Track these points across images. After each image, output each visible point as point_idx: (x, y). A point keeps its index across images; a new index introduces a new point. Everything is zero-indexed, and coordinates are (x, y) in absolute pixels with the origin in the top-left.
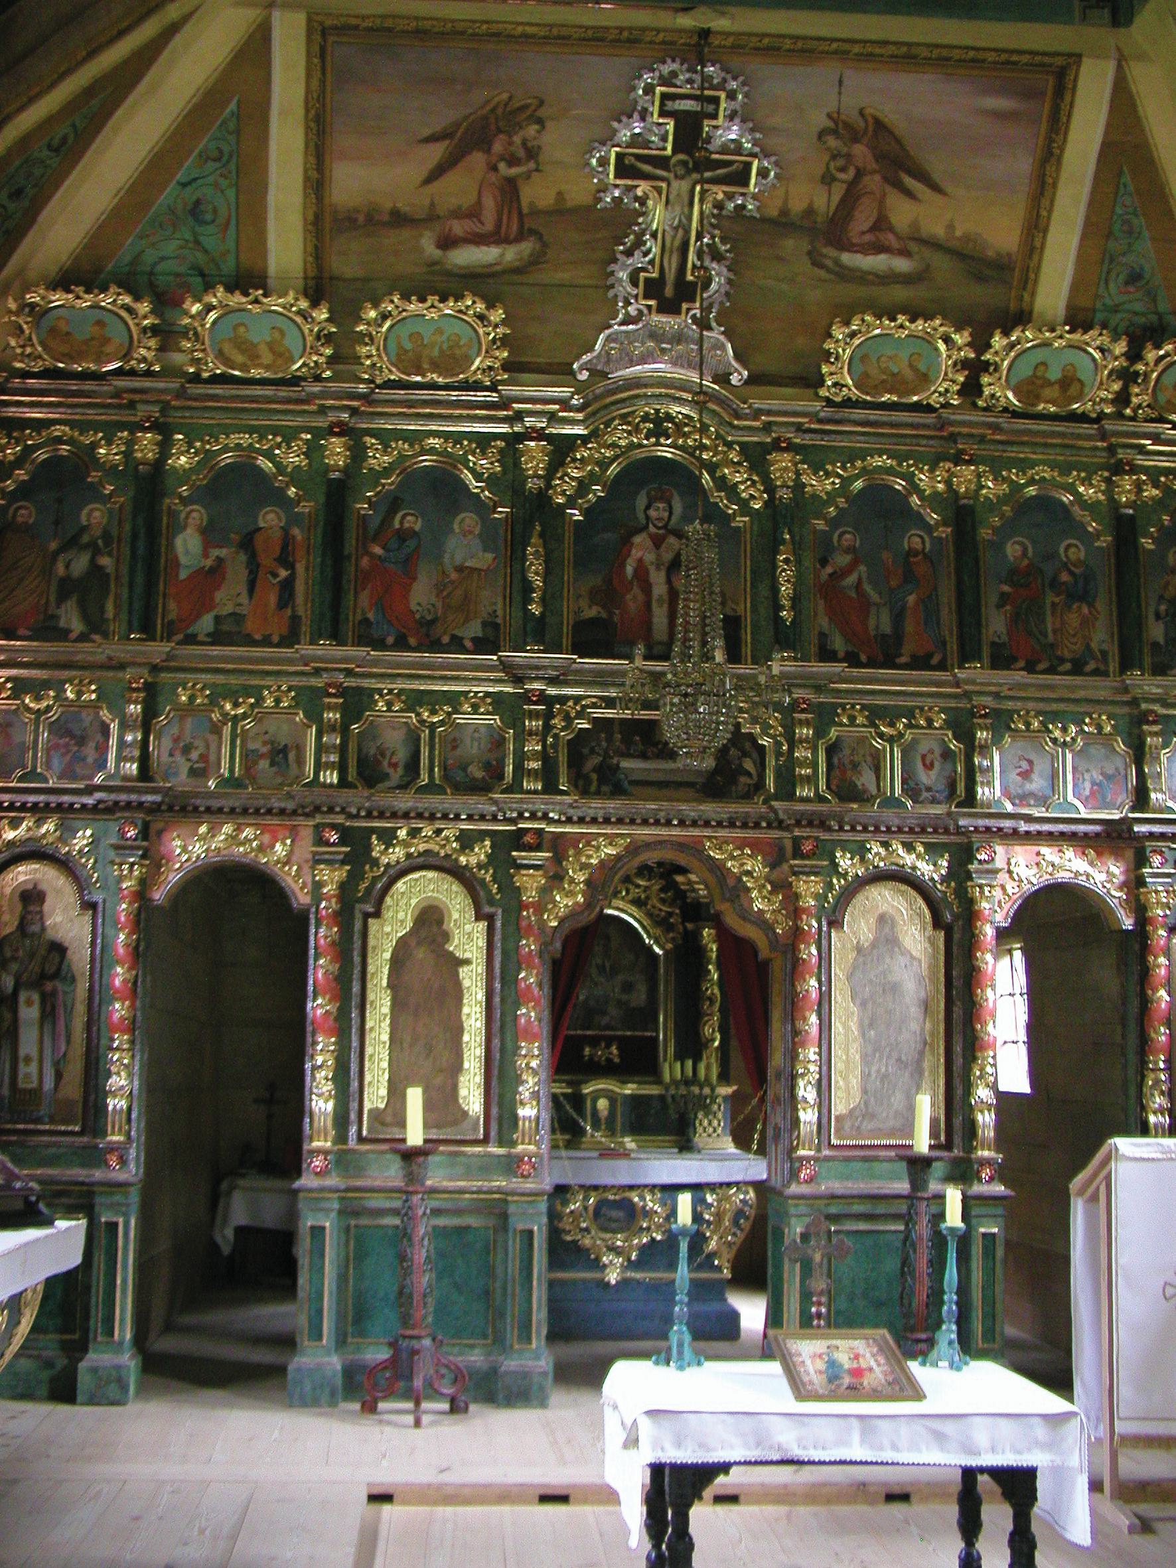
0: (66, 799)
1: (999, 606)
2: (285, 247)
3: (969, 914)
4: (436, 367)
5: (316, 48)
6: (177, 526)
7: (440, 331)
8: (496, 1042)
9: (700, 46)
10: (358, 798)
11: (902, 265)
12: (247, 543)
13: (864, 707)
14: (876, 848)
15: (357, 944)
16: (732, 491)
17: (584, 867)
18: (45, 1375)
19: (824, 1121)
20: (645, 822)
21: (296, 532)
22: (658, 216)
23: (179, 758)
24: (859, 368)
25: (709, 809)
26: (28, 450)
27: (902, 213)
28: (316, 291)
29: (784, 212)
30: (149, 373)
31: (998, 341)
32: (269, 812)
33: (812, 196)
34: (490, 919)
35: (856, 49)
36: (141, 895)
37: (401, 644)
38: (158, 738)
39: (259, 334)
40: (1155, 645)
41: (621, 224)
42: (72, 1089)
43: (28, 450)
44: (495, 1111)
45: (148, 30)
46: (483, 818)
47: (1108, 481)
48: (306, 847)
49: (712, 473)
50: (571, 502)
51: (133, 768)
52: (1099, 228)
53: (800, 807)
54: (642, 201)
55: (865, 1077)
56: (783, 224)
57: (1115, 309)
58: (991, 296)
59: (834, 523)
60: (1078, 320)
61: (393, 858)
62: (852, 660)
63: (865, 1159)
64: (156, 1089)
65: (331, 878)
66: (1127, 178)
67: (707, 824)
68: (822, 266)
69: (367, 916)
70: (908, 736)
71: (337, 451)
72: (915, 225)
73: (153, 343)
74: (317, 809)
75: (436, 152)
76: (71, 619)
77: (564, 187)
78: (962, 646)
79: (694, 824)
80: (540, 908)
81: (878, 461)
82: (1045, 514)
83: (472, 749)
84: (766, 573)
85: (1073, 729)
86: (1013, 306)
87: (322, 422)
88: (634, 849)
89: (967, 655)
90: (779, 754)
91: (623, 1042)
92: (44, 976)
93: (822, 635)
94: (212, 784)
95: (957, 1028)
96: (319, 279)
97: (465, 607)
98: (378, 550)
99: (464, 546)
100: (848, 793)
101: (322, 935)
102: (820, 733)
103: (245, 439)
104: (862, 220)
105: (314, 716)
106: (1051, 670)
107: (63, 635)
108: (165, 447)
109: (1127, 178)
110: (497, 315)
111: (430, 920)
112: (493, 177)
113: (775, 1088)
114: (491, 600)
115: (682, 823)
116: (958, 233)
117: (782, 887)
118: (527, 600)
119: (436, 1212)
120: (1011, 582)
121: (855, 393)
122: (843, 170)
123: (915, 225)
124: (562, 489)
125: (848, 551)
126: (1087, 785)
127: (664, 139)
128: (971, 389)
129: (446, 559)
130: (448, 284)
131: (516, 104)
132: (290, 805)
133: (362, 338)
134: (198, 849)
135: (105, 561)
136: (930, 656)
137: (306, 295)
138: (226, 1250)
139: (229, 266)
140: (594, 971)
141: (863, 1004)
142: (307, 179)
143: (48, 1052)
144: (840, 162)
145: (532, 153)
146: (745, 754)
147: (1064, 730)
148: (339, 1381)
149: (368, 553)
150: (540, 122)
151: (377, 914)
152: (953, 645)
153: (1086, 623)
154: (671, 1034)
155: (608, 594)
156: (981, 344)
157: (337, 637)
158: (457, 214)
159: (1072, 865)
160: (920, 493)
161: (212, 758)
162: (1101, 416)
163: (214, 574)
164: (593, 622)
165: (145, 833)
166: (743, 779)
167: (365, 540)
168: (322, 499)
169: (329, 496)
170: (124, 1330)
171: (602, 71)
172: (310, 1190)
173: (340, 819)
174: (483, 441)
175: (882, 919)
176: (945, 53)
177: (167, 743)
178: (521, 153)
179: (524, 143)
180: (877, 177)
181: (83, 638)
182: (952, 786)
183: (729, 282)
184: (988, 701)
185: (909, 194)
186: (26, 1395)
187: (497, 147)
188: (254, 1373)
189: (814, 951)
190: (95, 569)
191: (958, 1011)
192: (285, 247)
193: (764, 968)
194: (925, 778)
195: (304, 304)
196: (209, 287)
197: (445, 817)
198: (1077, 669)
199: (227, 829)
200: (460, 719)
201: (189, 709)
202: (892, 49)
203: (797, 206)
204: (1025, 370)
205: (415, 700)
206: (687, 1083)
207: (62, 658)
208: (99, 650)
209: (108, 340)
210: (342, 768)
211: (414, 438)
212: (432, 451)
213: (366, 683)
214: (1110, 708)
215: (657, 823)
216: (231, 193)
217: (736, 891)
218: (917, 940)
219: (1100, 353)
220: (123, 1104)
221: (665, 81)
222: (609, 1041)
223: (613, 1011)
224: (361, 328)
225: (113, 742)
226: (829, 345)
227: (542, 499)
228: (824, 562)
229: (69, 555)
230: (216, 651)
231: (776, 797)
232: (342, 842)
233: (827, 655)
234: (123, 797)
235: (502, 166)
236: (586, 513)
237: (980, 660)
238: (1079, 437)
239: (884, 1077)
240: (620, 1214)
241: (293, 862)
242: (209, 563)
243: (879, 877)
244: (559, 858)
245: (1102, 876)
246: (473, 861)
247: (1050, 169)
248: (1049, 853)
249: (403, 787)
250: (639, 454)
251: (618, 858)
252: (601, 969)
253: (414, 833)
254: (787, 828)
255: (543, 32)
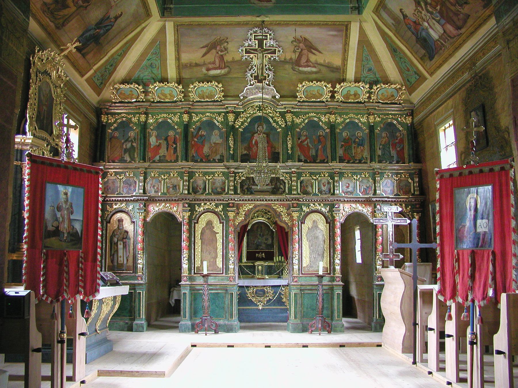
0: (127, 198)
1: (341, 148)
2: (172, 72)
3: (334, 220)
4: (207, 97)
5: (176, 29)
6: (150, 136)
7: (208, 89)
8: (225, 251)
9: (262, 25)
10: (191, 197)
11: (314, 70)
12: (166, 139)
13: (309, 172)
14: (312, 205)
15: (193, 230)
16: (277, 123)
17: (244, 211)
18: (126, 325)
19: (300, 268)
20: (258, 200)
21: (177, 136)
22: (255, 62)
23: (152, 188)
24: (305, 94)
25: (273, 197)
26: (116, 120)
27: (312, 58)
28: (179, 81)
29: (285, 59)
30: (143, 102)
31: (338, 86)
32: (172, 200)
33: (290, 55)
34: (223, 223)
35: (298, 23)
36: (144, 220)
37: (201, 161)
38: (147, 184)
39: (167, 92)
40: (379, 156)
41: (247, 65)
42: (130, 263)
43: (116, 120)
44: (224, 267)
45: (138, 29)
46: (220, 200)
47: (367, 117)
48: (181, 208)
49: (272, 119)
50: (240, 127)
51: (142, 191)
52: (359, 59)
53: (292, 196)
54: (252, 59)
55: (310, 258)
56: (285, 62)
57: (366, 77)
58: (336, 76)
59: (301, 129)
60: (357, 81)
61: (200, 210)
62: (306, 162)
63: (310, 277)
64: (149, 263)
65: (187, 215)
66: (365, 48)
67: (272, 200)
68: (295, 71)
69: (195, 223)
70: (319, 179)
71: (186, 118)
72: (316, 60)
73: (143, 95)
74: (183, 199)
75: (204, 50)
76: (127, 158)
77: (234, 56)
78: (332, 157)
79: (269, 200)
80: (234, 221)
81: (312, 114)
82: (353, 125)
83: (218, 184)
84: (285, 142)
85: (359, 176)
86: (341, 78)
87: (183, 111)
88: (255, 207)
89: (333, 159)
90: (289, 184)
91: (266, 253)
92: (123, 238)
93: (299, 156)
94: (160, 194)
95: (332, 246)
96: (180, 78)
97: (216, 152)
98: (196, 140)
99: (216, 138)
100: (305, 193)
101: (185, 228)
102: (298, 178)
103: (165, 115)
104: (303, 60)
105: (182, 178)
106: (353, 163)
107: (125, 161)
108: (147, 118)
109: (365, 48)
110: (220, 85)
111: (209, 223)
112: (217, 55)
113: (290, 261)
114: (222, 150)
115: (266, 200)
116: (327, 62)
117: (289, 214)
118: (230, 150)
119: (210, 289)
120: (344, 142)
121: (305, 99)
122: (298, 49)
123: (316, 60)
124: (238, 124)
125: (304, 136)
126: (363, 189)
127: (256, 45)
128: (333, 97)
129: (211, 141)
130: (208, 79)
131: (222, 39)
132: (177, 199)
133: (190, 92)
134: (157, 209)
135: (134, 144)
136: (324, 160)
137: (177, 83)
138: (173, 305)
139: (159, 77)
140: (258, 236)
141: (310, 241)
142: (176, 57)
143: (125, 255)
144: (297, 48)
145: (226, 49)
146: (281, 184)
147: (357, 176)
148: (190, 327)
149: (193, 140)
150: (227, 42)
151: (197, 223)
152: (330, 158)
153: (362, 151)
154: (277, 250)
155: (249, 148)
156: (334, 87)
157: (187, 160)
158: (210, 63)
159: (359, 208)
160: (322, 122)
161: (160, 188)
162: (365, 102)
163: (159, 147)
164: (245, 155)
165: (145, 206)
166: (281, 190)
167: (193, 137)
168: (183, 128)
169: (184, 128)
170: (143, 316)
171: (240, 31)
172: (183, 285)
173: (188, 201)
174: (219, 114)
175: (314, 221)
176: (319, 23)
177: (149, 185)
178: (224, 49)
179: (224, 47)
180: (306, 51)
181: (130, 162)
182: (330, 190)
183: (274, 75)
184: (338, 170)
185: (314, 54)
186: (123, 330)
187: (218, 48)
188: (174, 327)
189: (297, 229)
190: (132, 146)
191: (331, 242)
192: (172, 72)
193: (287, 233)
194: (323, 188)
195: (176, 85)
196: (155, 82)
197: (212, 200)
198: (360, 162)
199: (163, 204)
200: (215, 178)
201: (153, 178)
202: (306, 23)
203: (288, 58)
204: (345, 92)
205: (205, 174)
206: (279, 262)
207: (126, 167)
208: (134, 165)
209: (133, 95)
210: (188, 190)
211: (203, 113)
212: (208, 116)
213: (194, 170)
214: (368, 171)
215: (260, 200)
216: (159, 61)
217: (280, 216)
218: (323, 226)
219: (363, 88)
220: (141, 266)
221: (255, 32)
222: (262, 252)
223: (264, 245)
224: (190, 89)
225: (137, 185)
226: (298, 89)
227: (233, 127)
228: (299, 139)
229: (126, 143)
230: (159, 164)
231: (288, 194)
232: (189, 207)
233: (300, 161)
234: (140, 198)
235: (219, 52)
236: (244, 129)
237: (336, 160)
238: (360, 107)
239: (315, 258)
240: (262, 293)
241: (180, 212)
242: (158, 144)
243: (317, 211)
244: (238, 209)
245: (366, 210)
246: (219, 210)
247: (347, 47)
248: (354, 205)
249: (202, 194)
250: (255, 115)
251: (252, 209)
252: (260, 235)
253: (205, 204)
254: (290, 201)
255: (226, 23)
